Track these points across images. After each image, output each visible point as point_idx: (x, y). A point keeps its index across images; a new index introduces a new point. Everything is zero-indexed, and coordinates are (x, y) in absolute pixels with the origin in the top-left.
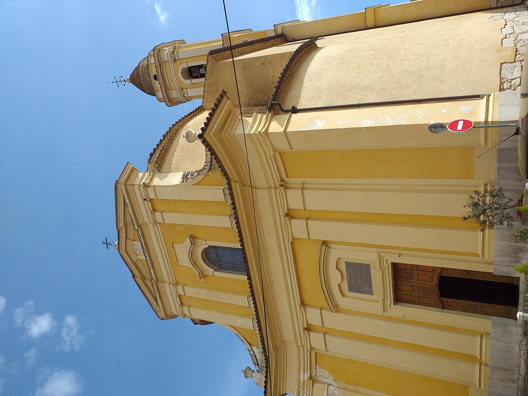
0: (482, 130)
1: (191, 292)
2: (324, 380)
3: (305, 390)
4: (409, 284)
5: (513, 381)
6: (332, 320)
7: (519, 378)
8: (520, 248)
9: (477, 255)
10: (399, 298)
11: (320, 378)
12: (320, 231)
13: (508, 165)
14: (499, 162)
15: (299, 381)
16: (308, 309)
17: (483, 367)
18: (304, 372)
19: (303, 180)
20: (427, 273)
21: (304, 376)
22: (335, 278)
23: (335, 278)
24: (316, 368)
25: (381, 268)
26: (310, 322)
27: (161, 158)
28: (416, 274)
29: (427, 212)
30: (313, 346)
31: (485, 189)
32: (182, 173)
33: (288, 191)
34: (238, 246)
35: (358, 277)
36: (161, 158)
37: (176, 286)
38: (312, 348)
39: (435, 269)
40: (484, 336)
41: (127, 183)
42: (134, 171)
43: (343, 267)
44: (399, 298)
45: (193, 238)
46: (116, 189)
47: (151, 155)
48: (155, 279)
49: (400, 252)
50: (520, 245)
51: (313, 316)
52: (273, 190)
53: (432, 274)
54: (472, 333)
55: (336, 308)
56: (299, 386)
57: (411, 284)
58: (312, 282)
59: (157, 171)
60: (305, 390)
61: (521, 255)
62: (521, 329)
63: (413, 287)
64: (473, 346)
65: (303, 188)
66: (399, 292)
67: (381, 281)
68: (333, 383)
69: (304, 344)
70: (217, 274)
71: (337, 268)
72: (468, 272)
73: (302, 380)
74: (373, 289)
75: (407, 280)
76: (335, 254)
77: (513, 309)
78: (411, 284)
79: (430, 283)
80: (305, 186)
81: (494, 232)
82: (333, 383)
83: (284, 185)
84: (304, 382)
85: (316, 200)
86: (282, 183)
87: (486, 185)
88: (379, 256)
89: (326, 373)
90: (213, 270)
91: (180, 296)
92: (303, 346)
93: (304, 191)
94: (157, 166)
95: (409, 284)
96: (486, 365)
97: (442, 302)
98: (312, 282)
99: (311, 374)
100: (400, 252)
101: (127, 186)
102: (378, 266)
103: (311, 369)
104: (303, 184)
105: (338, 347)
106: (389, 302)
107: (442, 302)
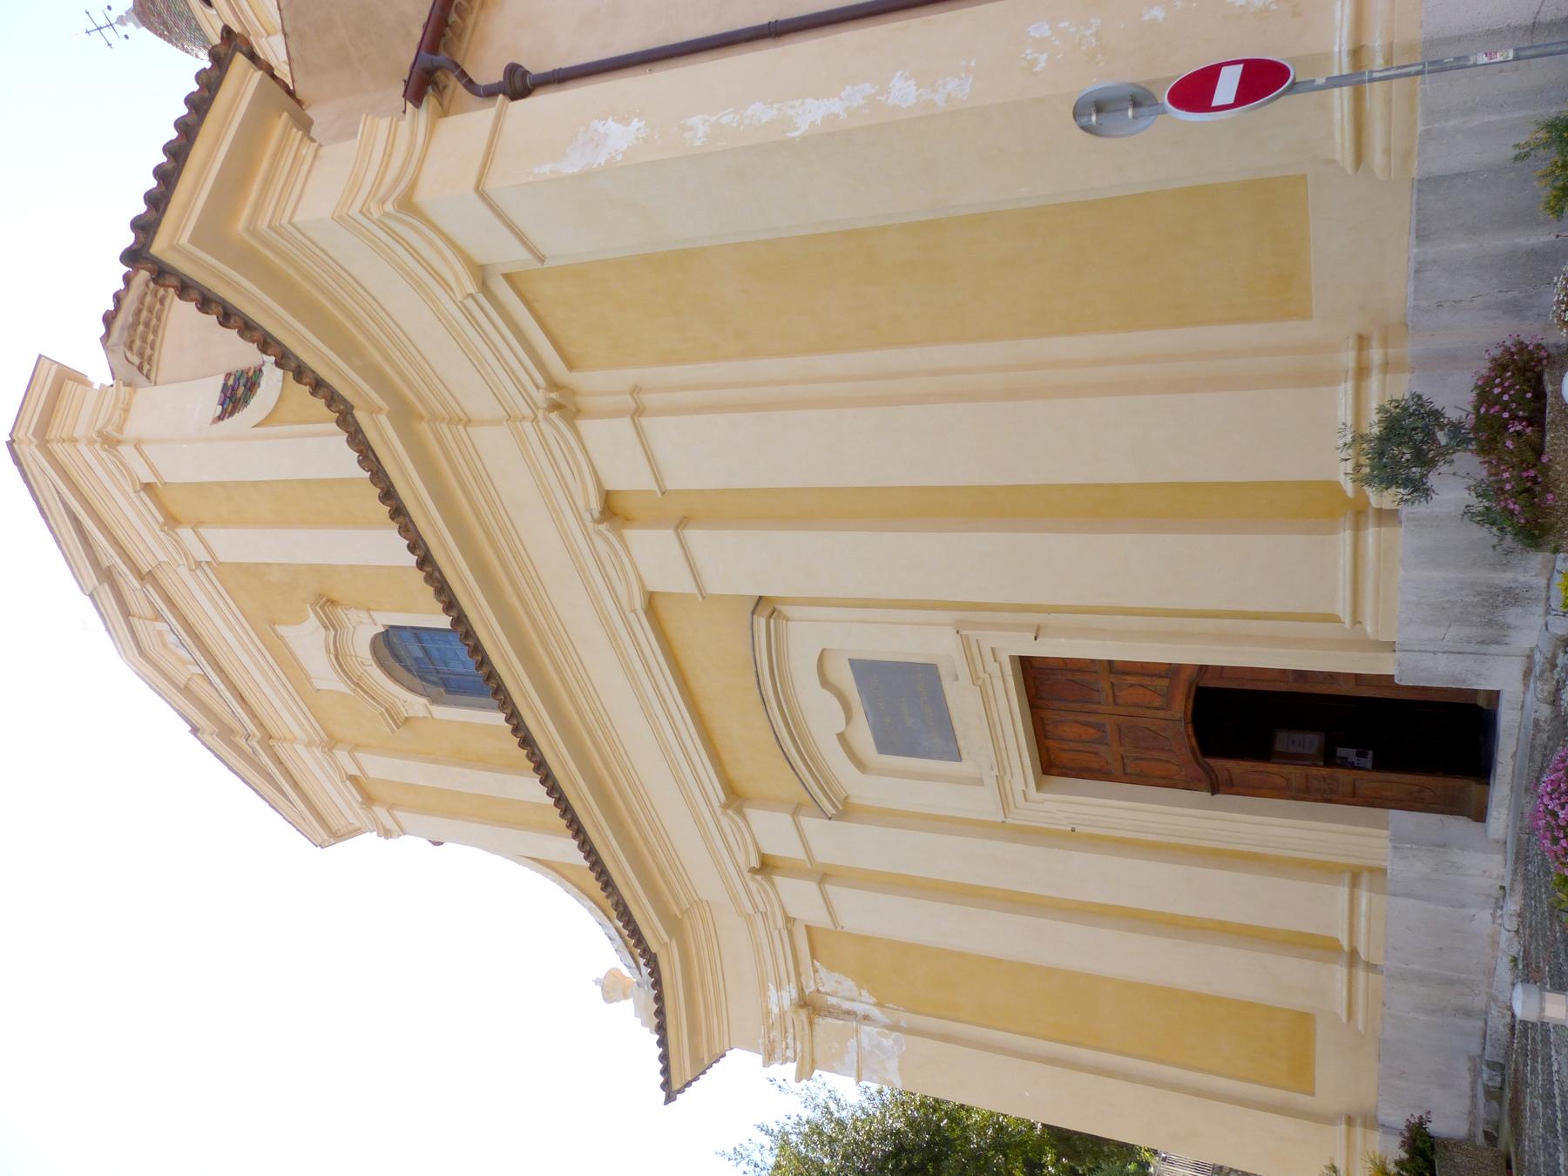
0: (1341, 99)
1: (377, 767)
2: (847, 1005)
3: (790, 1037)
4: (1077, 717)
5: (1468, 1014)
6: (832, 842)
7: (1488, 1006)
8: (1508, 591)
9: (1335, 619)
10: (1054, 761)
11: (832, 1000)
12: (737, 562)
13: (1463, 246)
14: (1422, 234)
15: (768, 1012)
16: (750, 812)
17: (1361, 975)
18: (779, 987)
19: (631, 375)
20: (1146, 681)
21: (780, 999)
22: (823, 716)
23: (823, 716)
24: (815, 971)
25: (975, 678)
26: (767, 850)
27: (147, 325)
28: (1106, 686)
29: (1128, 474)
30: (792, 914)
31: (1359, 358)
32: (218, 382)
33: (584, 425)
34: (1214, 104)
35: (904, 706)
36: (147, 325)
37: (330, 750)
38: (789, 921)
39: (1173, 671)
40: (1365, 878)
41: (53, 434)
42: (70, 385)
43: (845, 678)
44: (1054, 761)
45: (327, 604)
46: (17, 460)
47: (109, 319)
48: (258, 735)
49: (1037, 618)
50: (1506, 578)
51: (773, 831)
52: (528, 425)
53: (1165, 682)
54: (1323, 870)
55: (845, 811)
56: (770, 1028)
57: (1092, 719)
58: (741, 727)
59: (141, 379)
60: (790, 1037)
61: (1513, 615)
62: (1500, 858)
63: (1100, 728)
64: (1324, 908)
65: (638, 412)
66: (1051, 743)
67: (992, 720)
68: (875, 1012)
69: (762, 909)
70: (444, 713)
71: (825, 682)
72: (1301, 675)
73: (775, 1010)
74: (961, 743)
75: (1076, 706)
76: (804, 640)
77: (1474, 788)
78: (1092, 719)
79: (1161, 714)
80: (649, 399)
81: (1400, 538)
82: (875, 1012)
83: (565, 406)
84: (782, 1014)
85: (699, 452)
86: (553, 395)
87: (1362, 341)
88: (966, 644)
89: (849, 983)
90: (424, 701)
91: (353, 779)
92: (764, 915)
93: (645, 421)
94: (136, 360)
95: (1077, 717)
96: (1371, 967)
97: (1209, 772)
98: (741, 727)
99: (801, 990)
100: (1037, 618)
101: (56, 448)
102: (964, 672)
103: (798, 975)
104: (636, 390)
105: (861, 913)
106: (1019, 786)
107: (1209, 772)
